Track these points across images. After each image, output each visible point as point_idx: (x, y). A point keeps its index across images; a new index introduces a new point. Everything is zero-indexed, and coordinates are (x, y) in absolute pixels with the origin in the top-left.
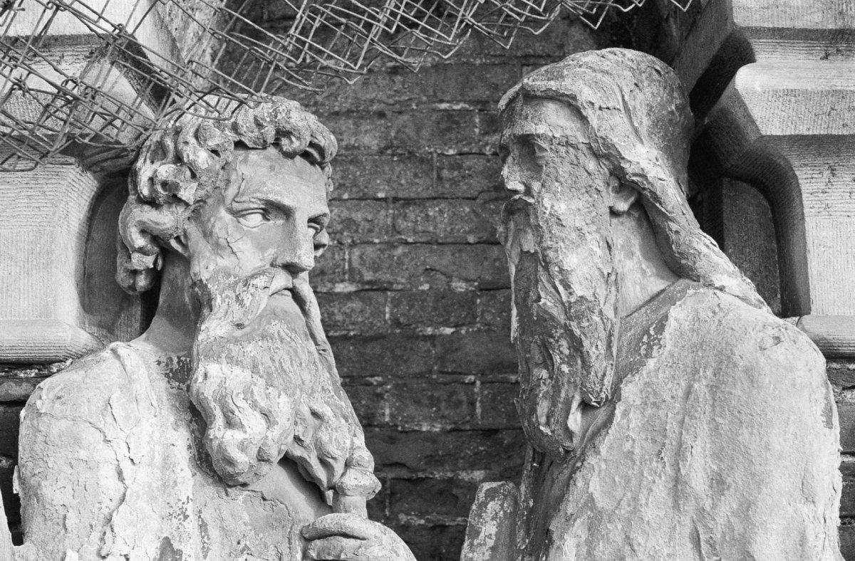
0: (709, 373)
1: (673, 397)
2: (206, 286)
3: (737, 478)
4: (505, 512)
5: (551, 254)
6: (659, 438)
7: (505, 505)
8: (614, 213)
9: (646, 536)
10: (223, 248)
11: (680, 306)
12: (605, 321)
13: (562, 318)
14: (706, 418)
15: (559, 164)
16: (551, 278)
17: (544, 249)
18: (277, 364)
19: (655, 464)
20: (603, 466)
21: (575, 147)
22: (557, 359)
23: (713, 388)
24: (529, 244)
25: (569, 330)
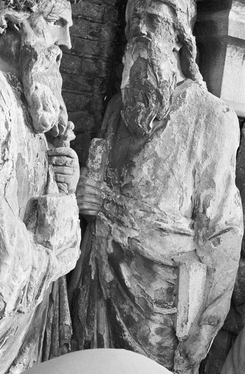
0: (205, 116)
1: (191, 123)
2: (34, 49)
3: (212, 154)
4: (104, 151)
5: (155, 62)
6: (185, 136)
7: (104, 148)
8: (174, 50)
9: (178, 170)
10: (40, 33)
11: (190, 89)
12: (171, 90)
13: (156, 87)
14: (203, 132)
15: (162, 28)
16: (153, 71)
17: (153, 59)
18: (55, 86)
19: (183, 145)
20: (162, 142)
21: (169, 24)
22: (151, 100)
23: (206, 123)
24: (145, 55)
25: (158, 92)
